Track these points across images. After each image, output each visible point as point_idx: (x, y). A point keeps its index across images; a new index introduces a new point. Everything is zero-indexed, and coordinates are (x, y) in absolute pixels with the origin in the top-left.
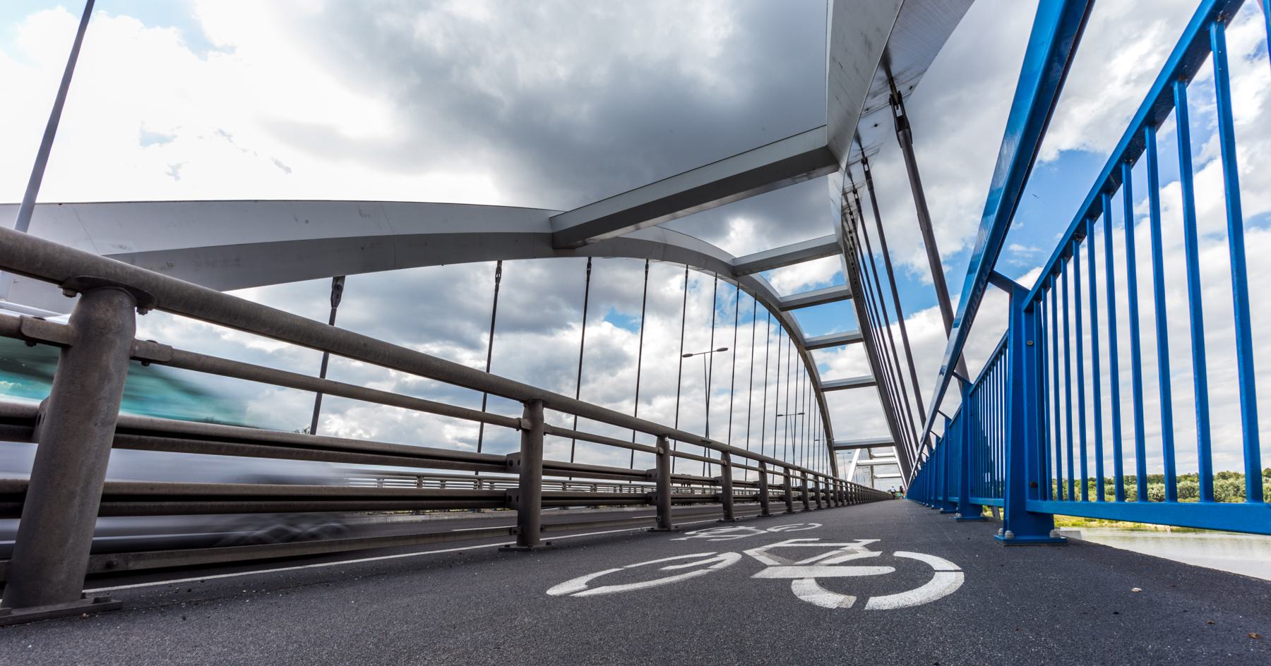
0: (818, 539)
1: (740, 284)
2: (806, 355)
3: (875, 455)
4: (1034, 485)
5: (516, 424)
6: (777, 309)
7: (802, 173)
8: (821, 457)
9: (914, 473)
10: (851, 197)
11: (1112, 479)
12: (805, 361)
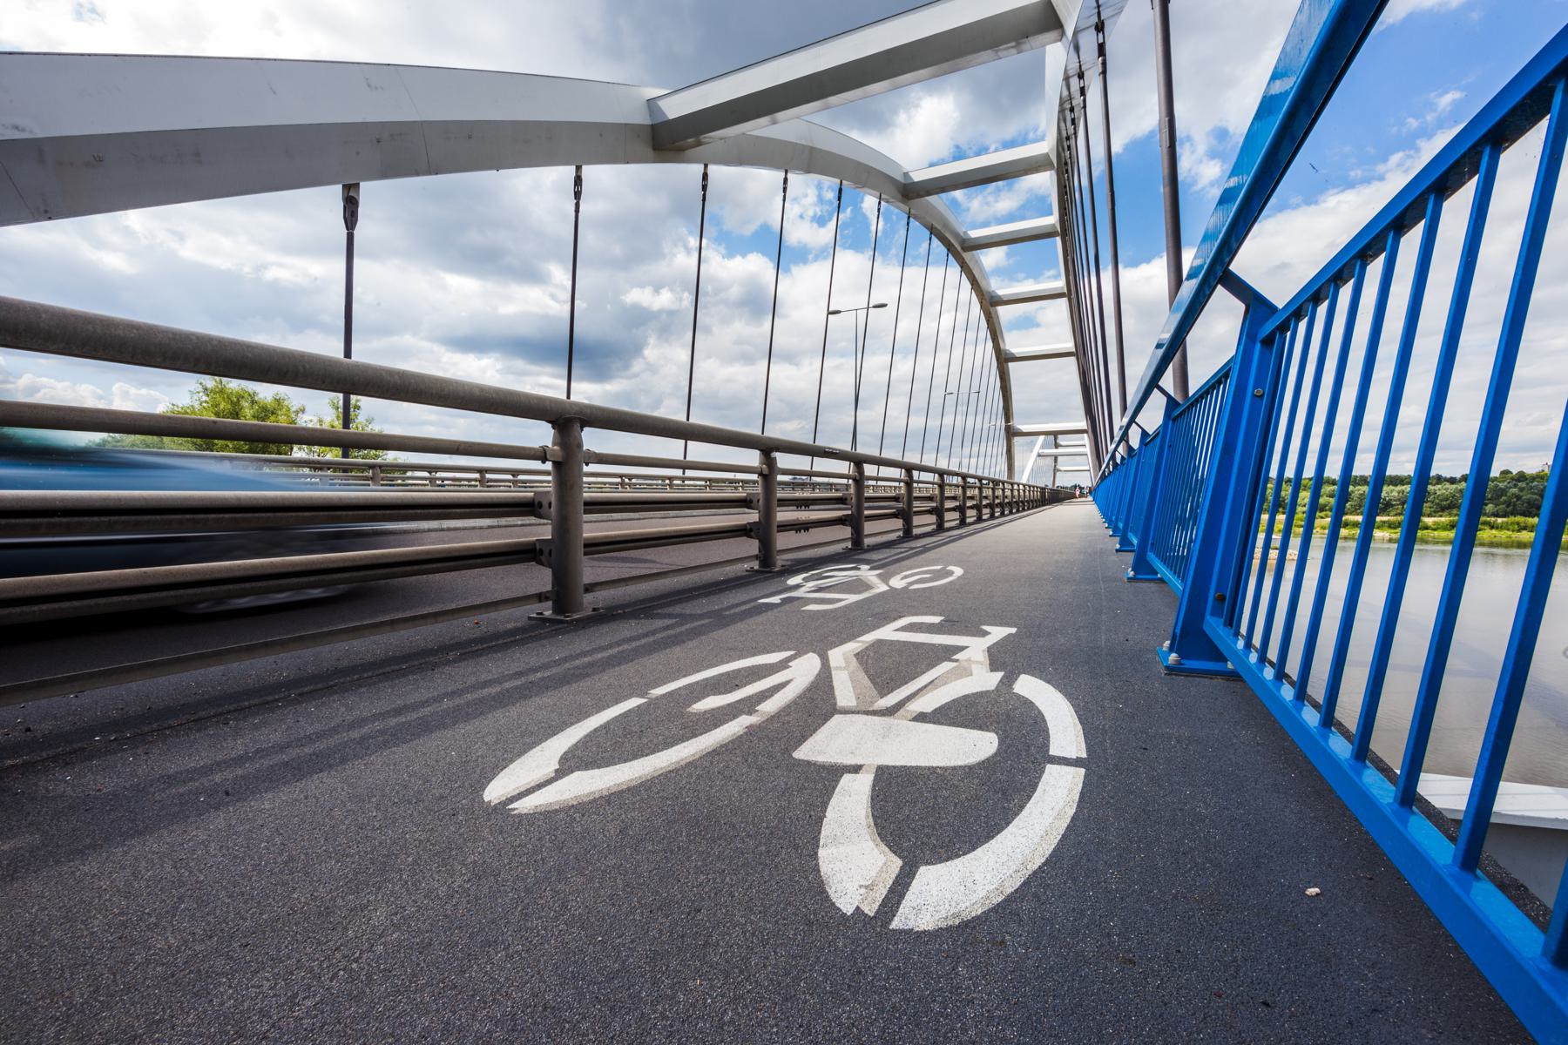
0: (936, 619)
1: (912, 211)
2: (990, 313)
3: (1062, 443)
4: (1221, 599)
5: (542, 455)
6: (959, 248)
7: (1009, 43)
8: (996, 444)
9: (1108, 464)
10: (1075, 84)
11: (1337, 479)
12: (988, 321)
